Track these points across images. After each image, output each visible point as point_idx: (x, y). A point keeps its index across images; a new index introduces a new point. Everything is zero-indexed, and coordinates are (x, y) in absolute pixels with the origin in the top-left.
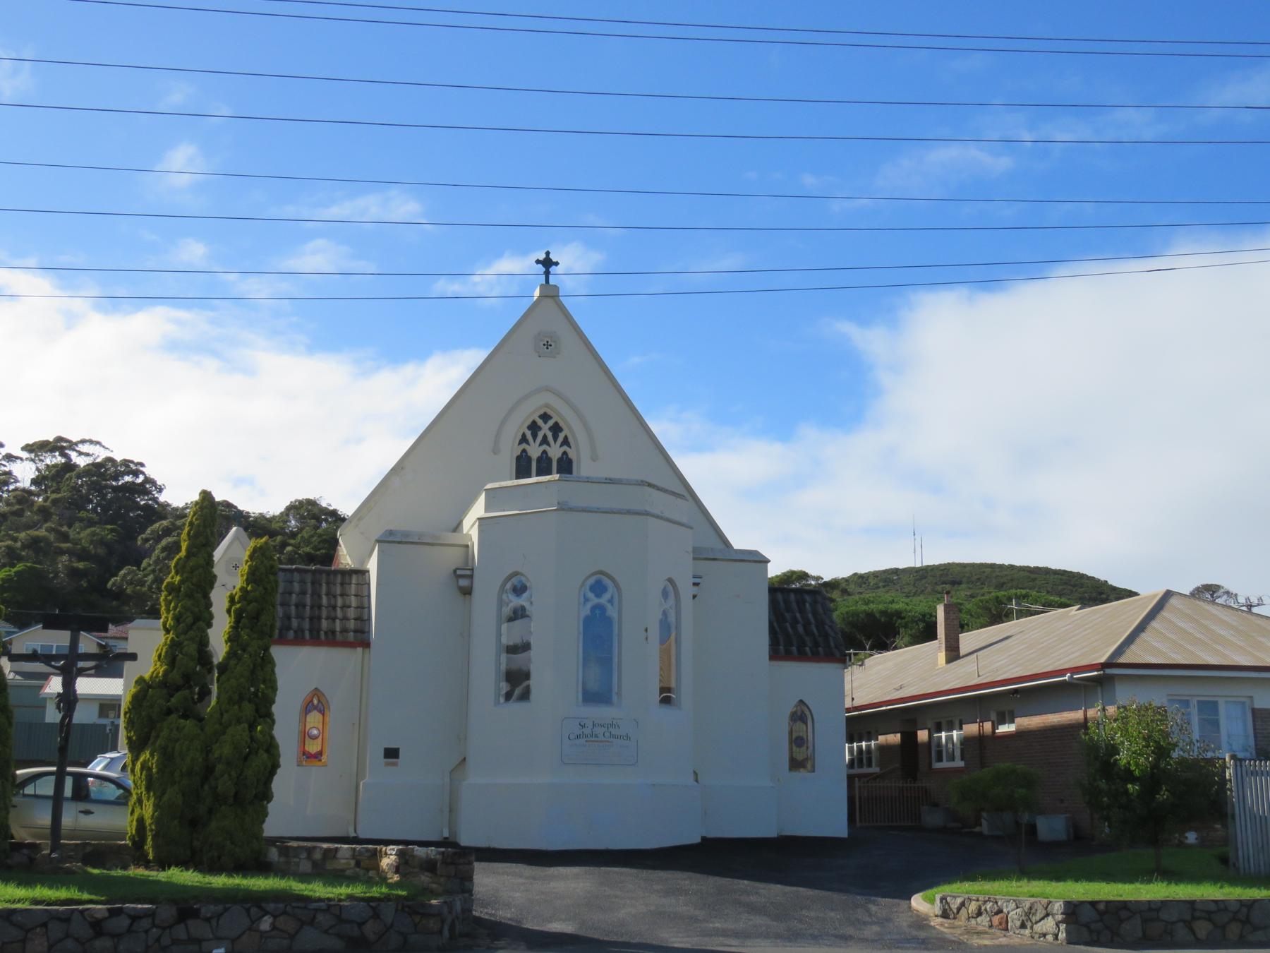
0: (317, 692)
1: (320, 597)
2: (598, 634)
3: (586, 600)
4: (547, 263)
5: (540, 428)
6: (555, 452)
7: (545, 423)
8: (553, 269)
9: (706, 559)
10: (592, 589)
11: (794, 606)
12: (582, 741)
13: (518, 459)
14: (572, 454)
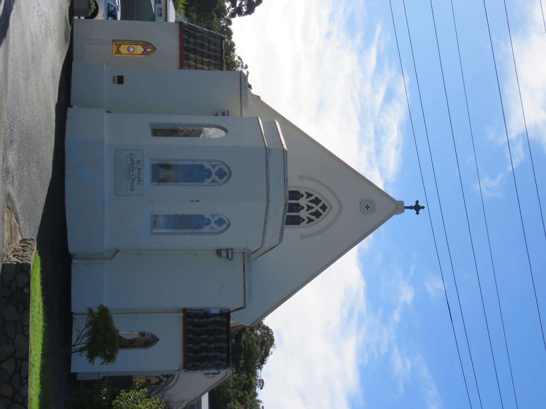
0: (154, 49)
1: (208, 58)
2: (195, 173)
3: (214, 166)
4: (417, 208)
5: (317, 205)
6: (304, 214)
7: (321, 208)
8: (414, 211)
9: (244, 265)
10: (220, 170)
11: (218, 345)
12: (130, 162)
13: (297, 192)
14: (304, 224)
